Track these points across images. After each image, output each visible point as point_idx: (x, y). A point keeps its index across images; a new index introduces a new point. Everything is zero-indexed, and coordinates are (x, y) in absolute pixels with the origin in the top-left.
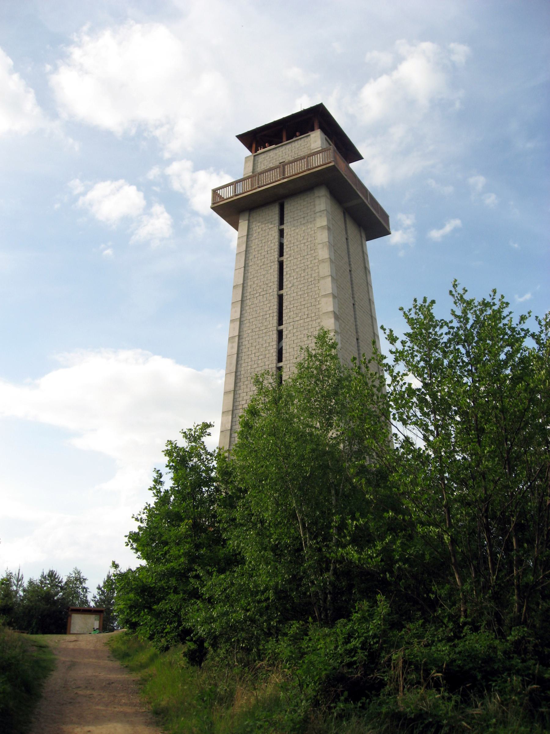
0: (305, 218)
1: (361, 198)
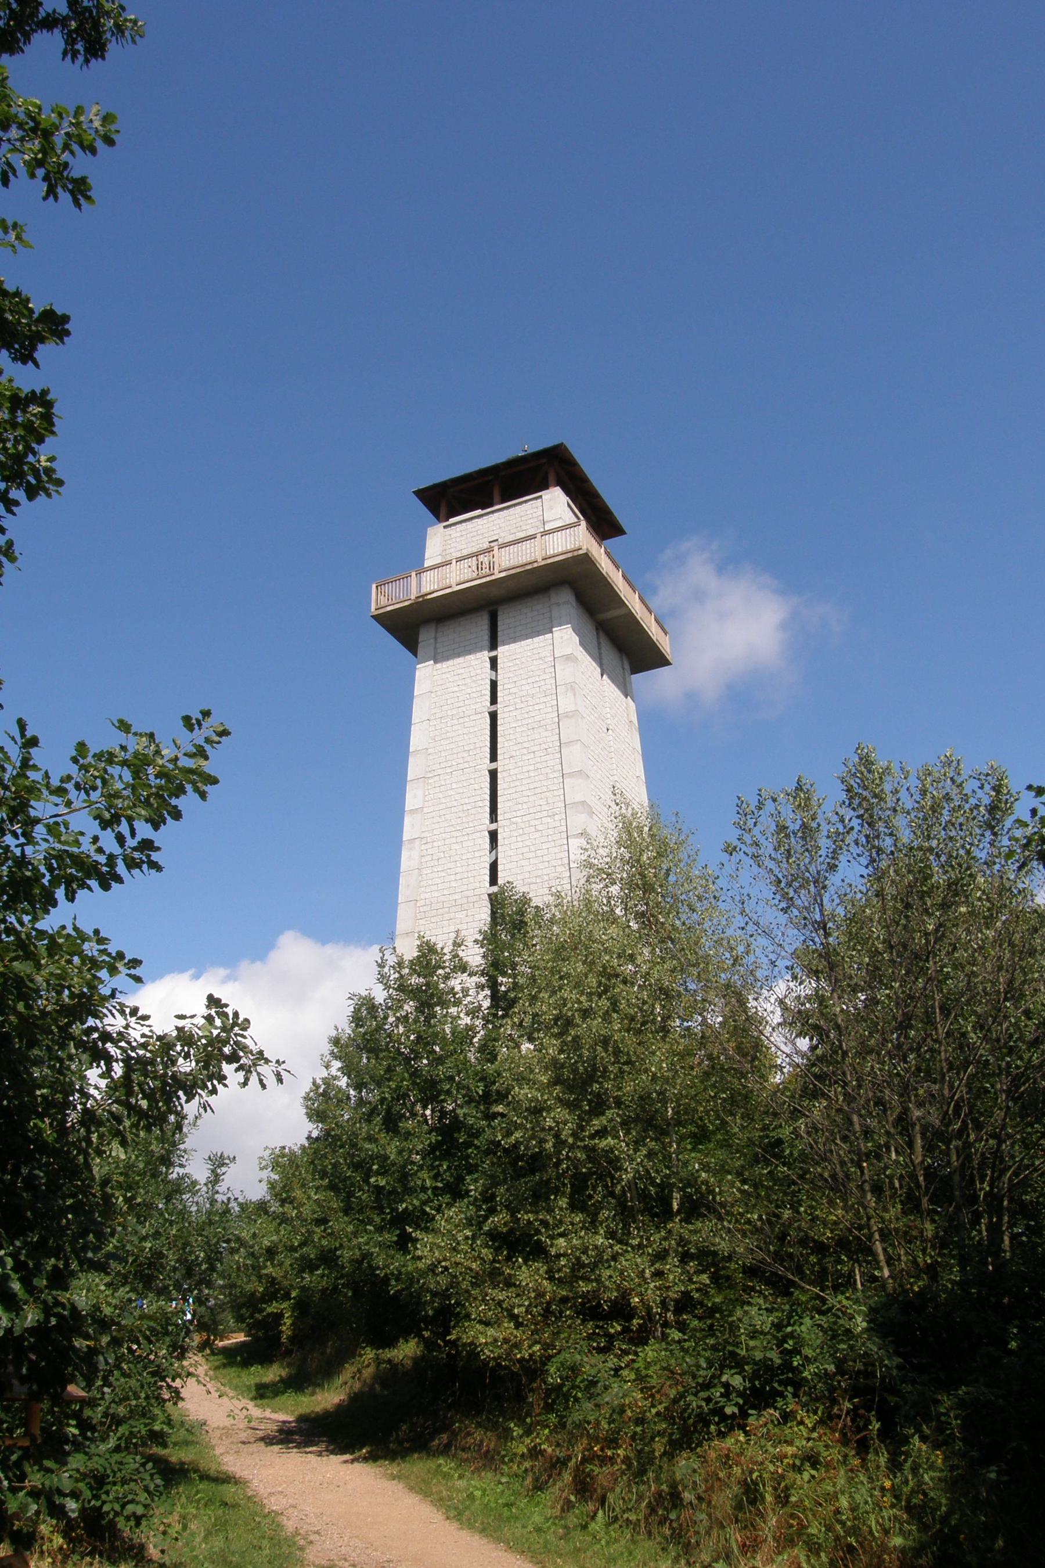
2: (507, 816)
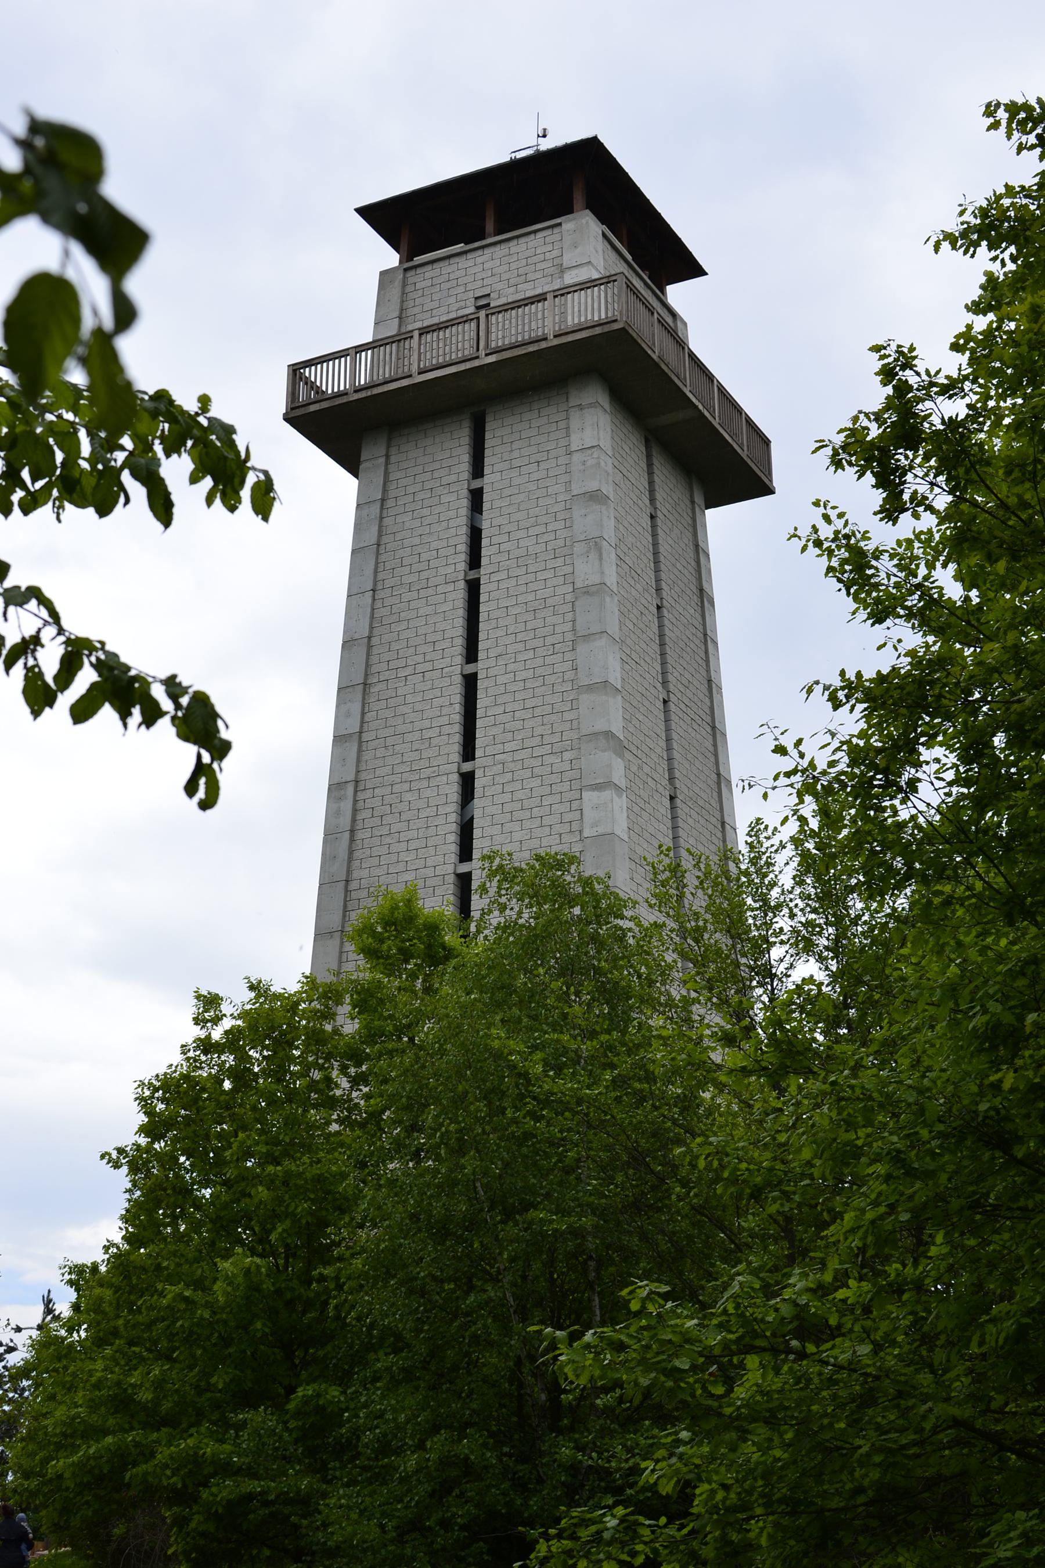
0: (543, 466)
1: (696, 407)
2: (490, 751)
